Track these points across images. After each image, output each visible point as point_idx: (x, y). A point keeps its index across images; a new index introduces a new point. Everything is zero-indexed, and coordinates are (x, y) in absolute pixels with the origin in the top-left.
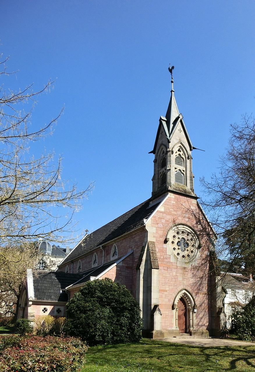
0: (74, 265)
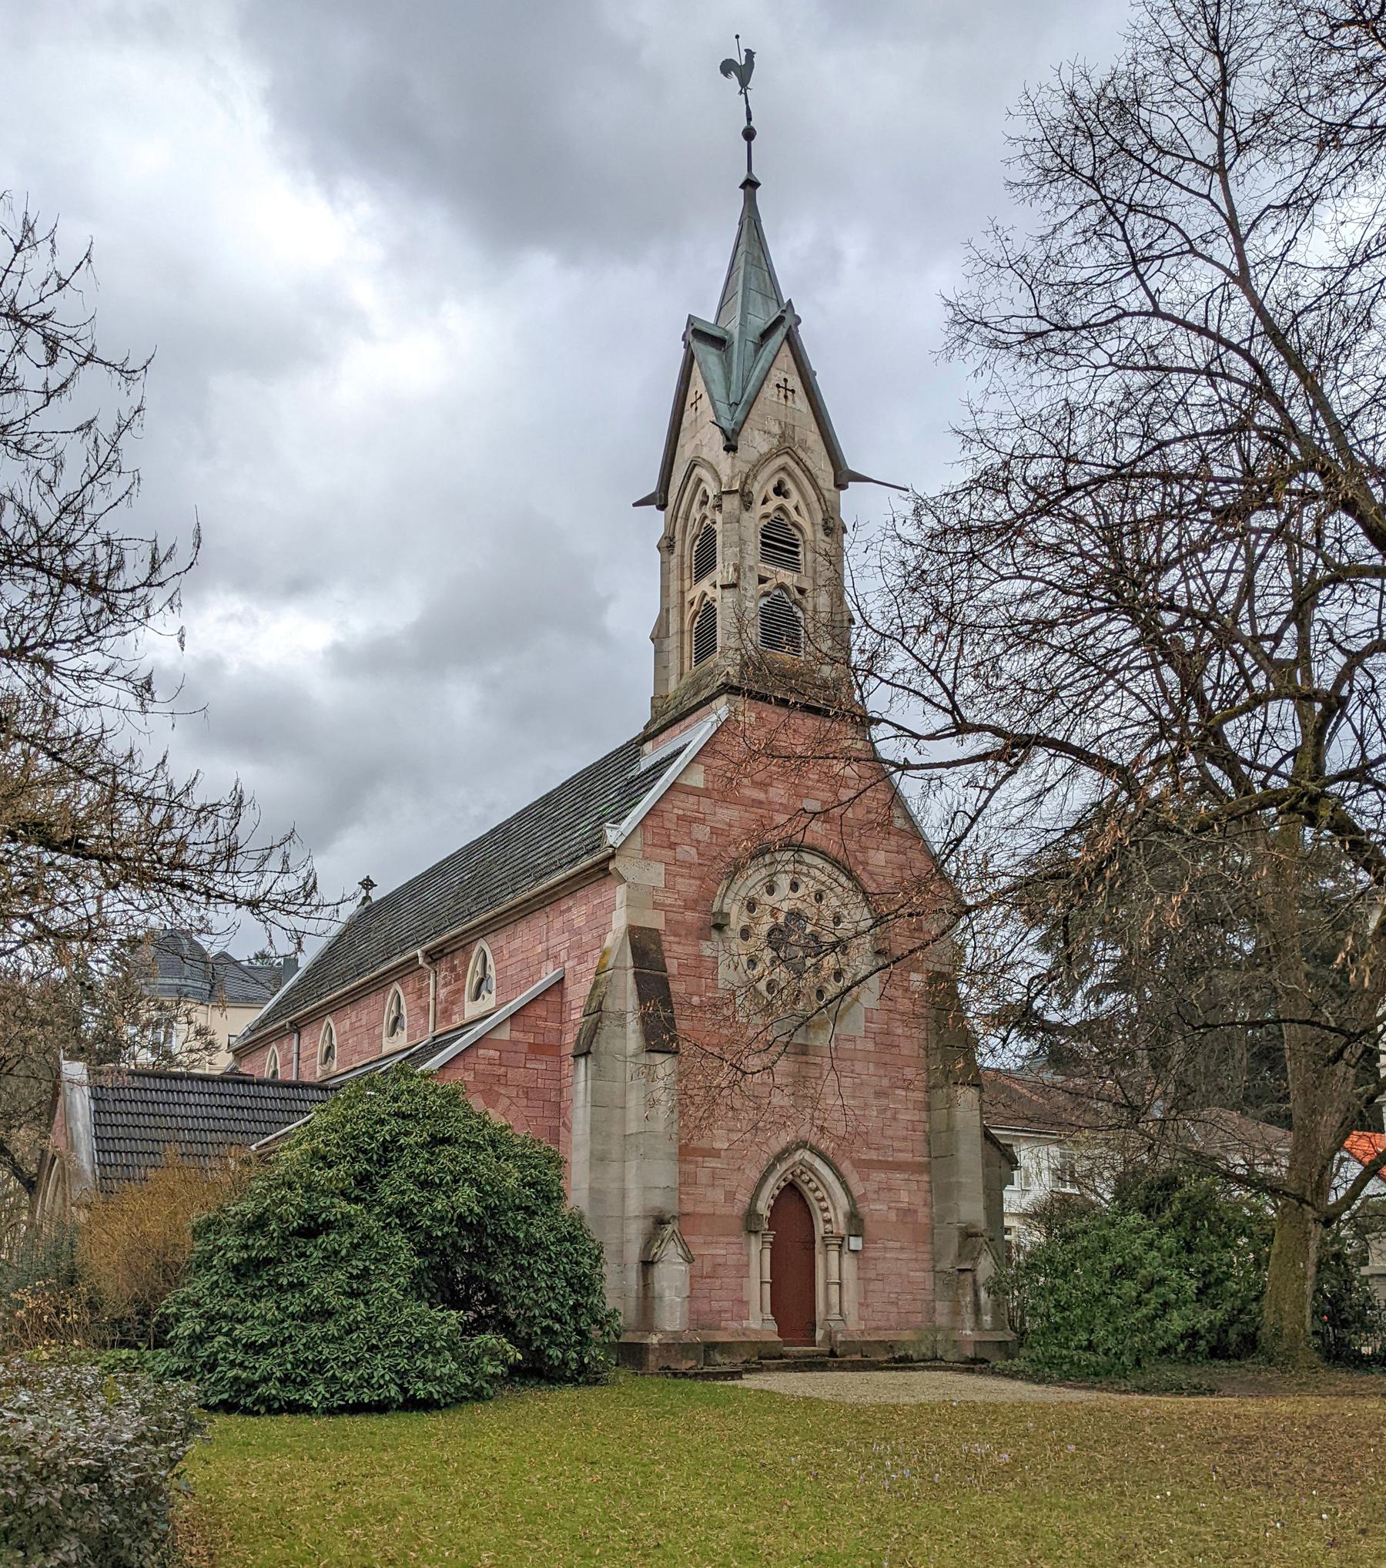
0: (306, 1040)
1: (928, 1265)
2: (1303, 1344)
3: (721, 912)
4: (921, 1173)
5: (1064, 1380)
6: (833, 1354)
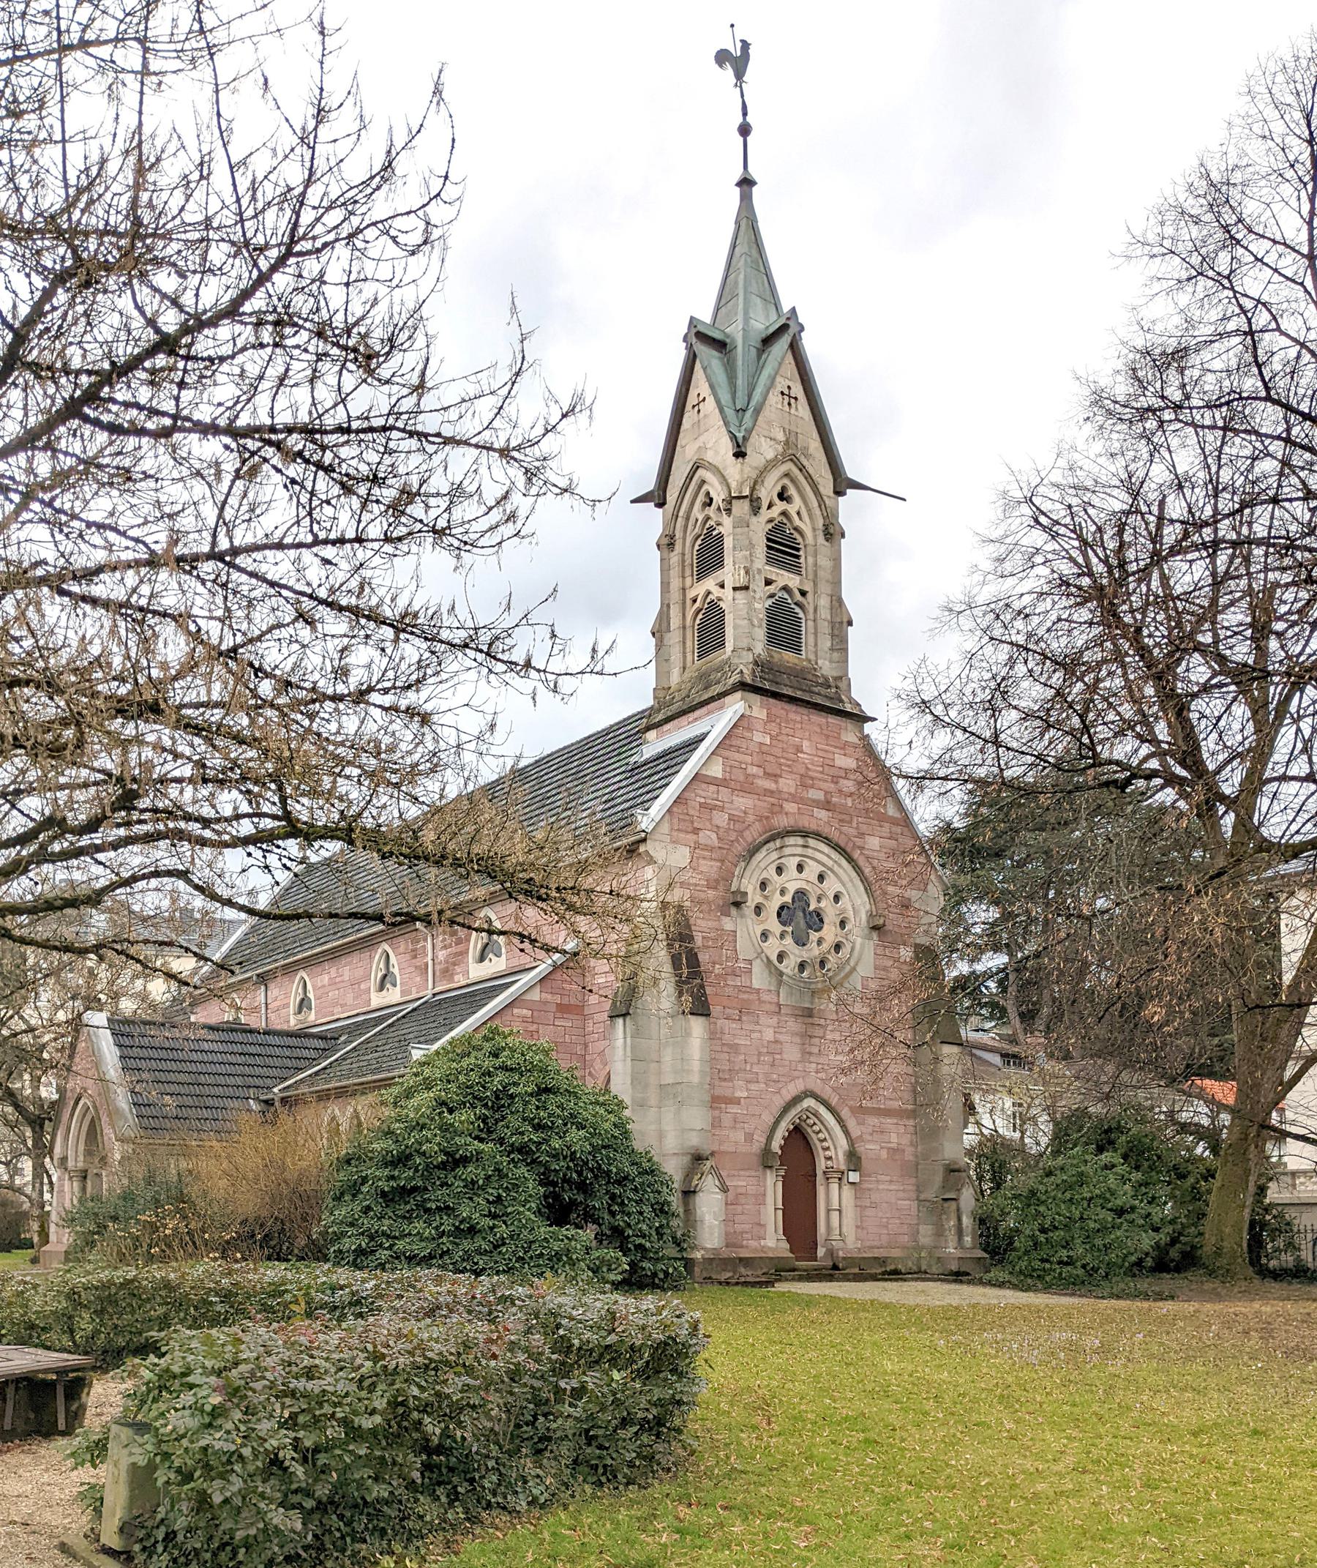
1: (914, 1196)
2: (1240, 1260)
3: (738, 892)
4: (908, 1118)
5: (1047, 1288)
6: (835, 1267)
